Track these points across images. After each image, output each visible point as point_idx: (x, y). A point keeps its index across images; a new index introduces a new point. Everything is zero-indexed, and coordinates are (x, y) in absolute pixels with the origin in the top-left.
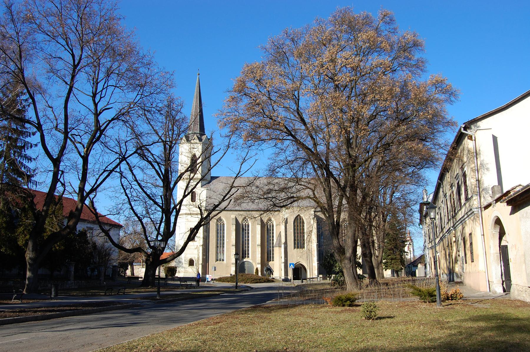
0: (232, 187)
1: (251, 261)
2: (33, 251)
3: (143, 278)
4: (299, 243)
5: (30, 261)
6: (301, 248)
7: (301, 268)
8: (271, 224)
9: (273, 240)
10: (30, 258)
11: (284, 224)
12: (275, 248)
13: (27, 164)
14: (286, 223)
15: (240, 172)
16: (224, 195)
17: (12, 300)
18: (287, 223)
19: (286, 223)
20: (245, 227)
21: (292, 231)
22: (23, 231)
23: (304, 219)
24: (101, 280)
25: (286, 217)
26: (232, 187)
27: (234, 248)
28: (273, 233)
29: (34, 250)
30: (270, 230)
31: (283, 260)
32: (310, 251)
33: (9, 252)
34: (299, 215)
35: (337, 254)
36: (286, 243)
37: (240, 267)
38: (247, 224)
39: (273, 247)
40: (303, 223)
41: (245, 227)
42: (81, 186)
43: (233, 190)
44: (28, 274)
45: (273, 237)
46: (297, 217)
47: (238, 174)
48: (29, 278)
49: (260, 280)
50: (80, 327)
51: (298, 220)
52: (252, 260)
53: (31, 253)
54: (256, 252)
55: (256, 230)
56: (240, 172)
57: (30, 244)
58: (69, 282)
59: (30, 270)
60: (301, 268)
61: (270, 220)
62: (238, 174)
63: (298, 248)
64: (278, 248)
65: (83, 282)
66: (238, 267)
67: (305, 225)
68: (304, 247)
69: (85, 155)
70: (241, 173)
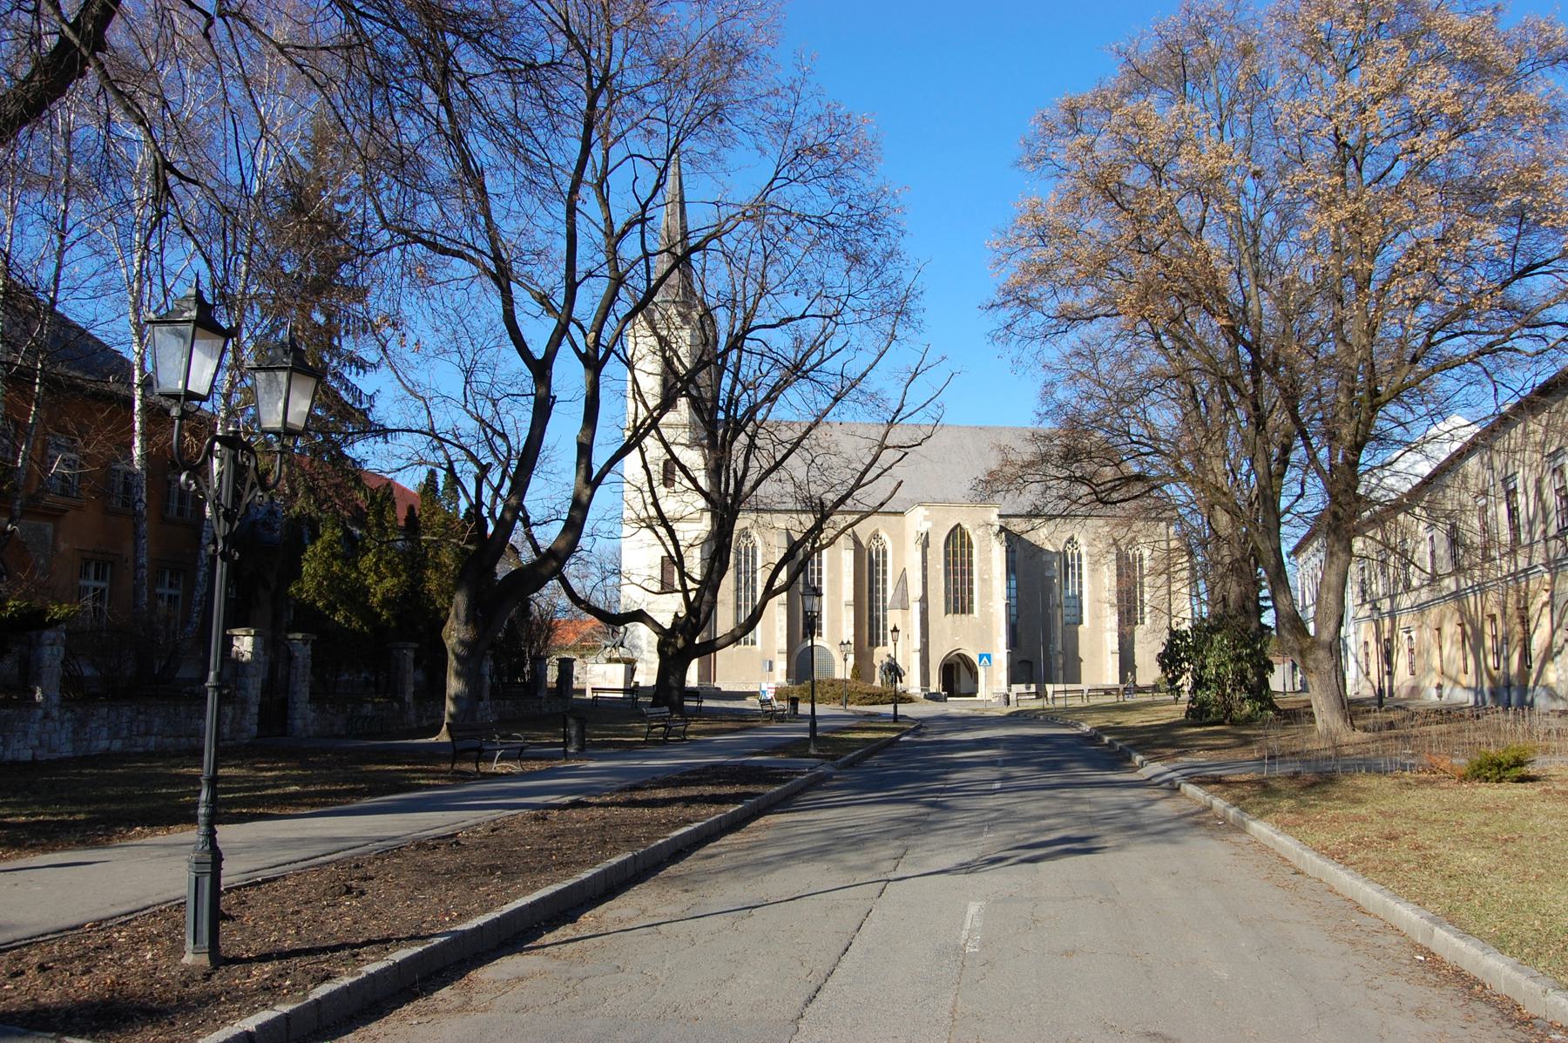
0: (883, 447)
1: (827, 646)
2: (466, 623)
3: (956, 706)
4: (960, 602)
5: (459, 649)
6: (963, 612)
7: (958, 664)
8: (750, 546)
9: (884, 590)
10: (462, 642)
11: (920, 548)
12: (889, 613)
13: (353, 379)
14: (925, 545)
15: (902, 406)
16: (862, 468)
17: (492, 761)
18: (928, 546)
19: (925, 545)
20: (1073, 559)
21: (941, 566)
22: (376, 564)
23: (973, 537)
24: (541, 698)
25: (923, 530)
26: (883, 447)
27: (851, 609)
28: (885, 572)
29: (471, 619)
30: (878, 565)
31: (917, 645)
32: (987, 617)
33: (355, 624)
34: (959, 525)
35: (1290, 634)
36: (924, 600)
37: (802, 663)
38: (1076, 552)
39: (885, 610)
40: (970, 545)
41: (1073, 559)
42: (585, 440)
43: (888, 457)
44: (454, 685)
45: (885, 581)
46: (953, 530)
47: (898, 411)
48: (456, 699)
49: (880, 695)
50: (966, 856)
51: (955, 537)
52: (829, 642)
53: (462, 628)
54: (840, 621)
55: (840, 564)
56: (902, 406)
57: (460, 600)
58: (481, 704)
59: (458, 674)
60: (958, 664)
61: (876, 536)
62: (898, 411)
63: (956, 612)
64: (898, 612)
65: (508, 703)
66: (794, 659)
67: (975, 552)
68: (971, 611)
69: (591, 352)
70: (906, 411)
